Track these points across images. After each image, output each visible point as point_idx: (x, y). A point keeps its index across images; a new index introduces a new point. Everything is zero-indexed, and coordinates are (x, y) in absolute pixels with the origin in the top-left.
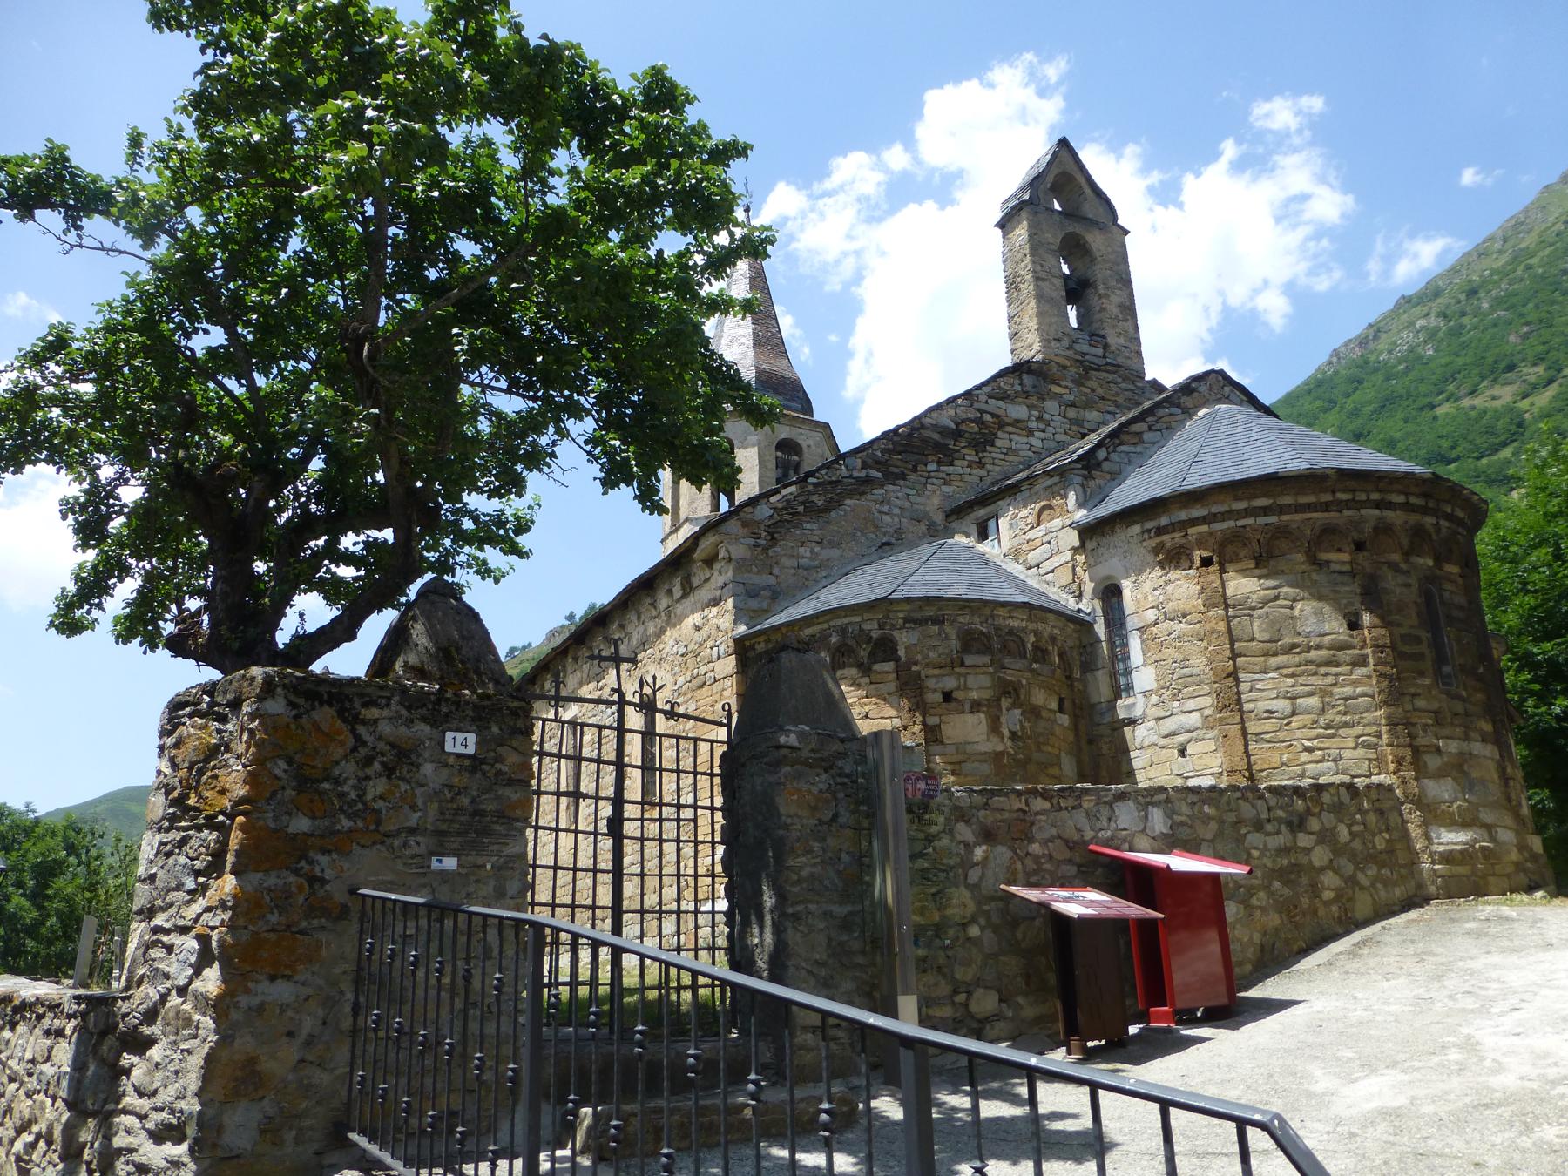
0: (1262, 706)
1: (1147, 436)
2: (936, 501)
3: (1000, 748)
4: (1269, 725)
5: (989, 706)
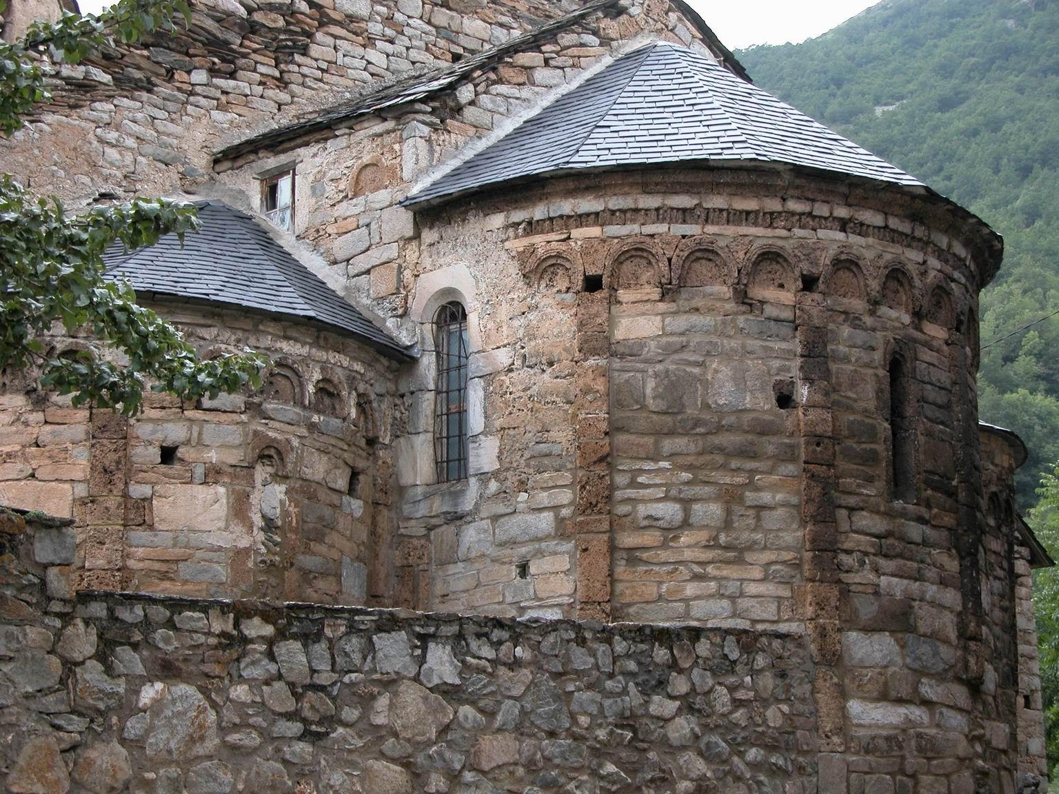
0: (642, 510)
1: (541, 75)
2: (200, 135)
3: (244, 543)
4: (650, 538)
5: (234, 477)
